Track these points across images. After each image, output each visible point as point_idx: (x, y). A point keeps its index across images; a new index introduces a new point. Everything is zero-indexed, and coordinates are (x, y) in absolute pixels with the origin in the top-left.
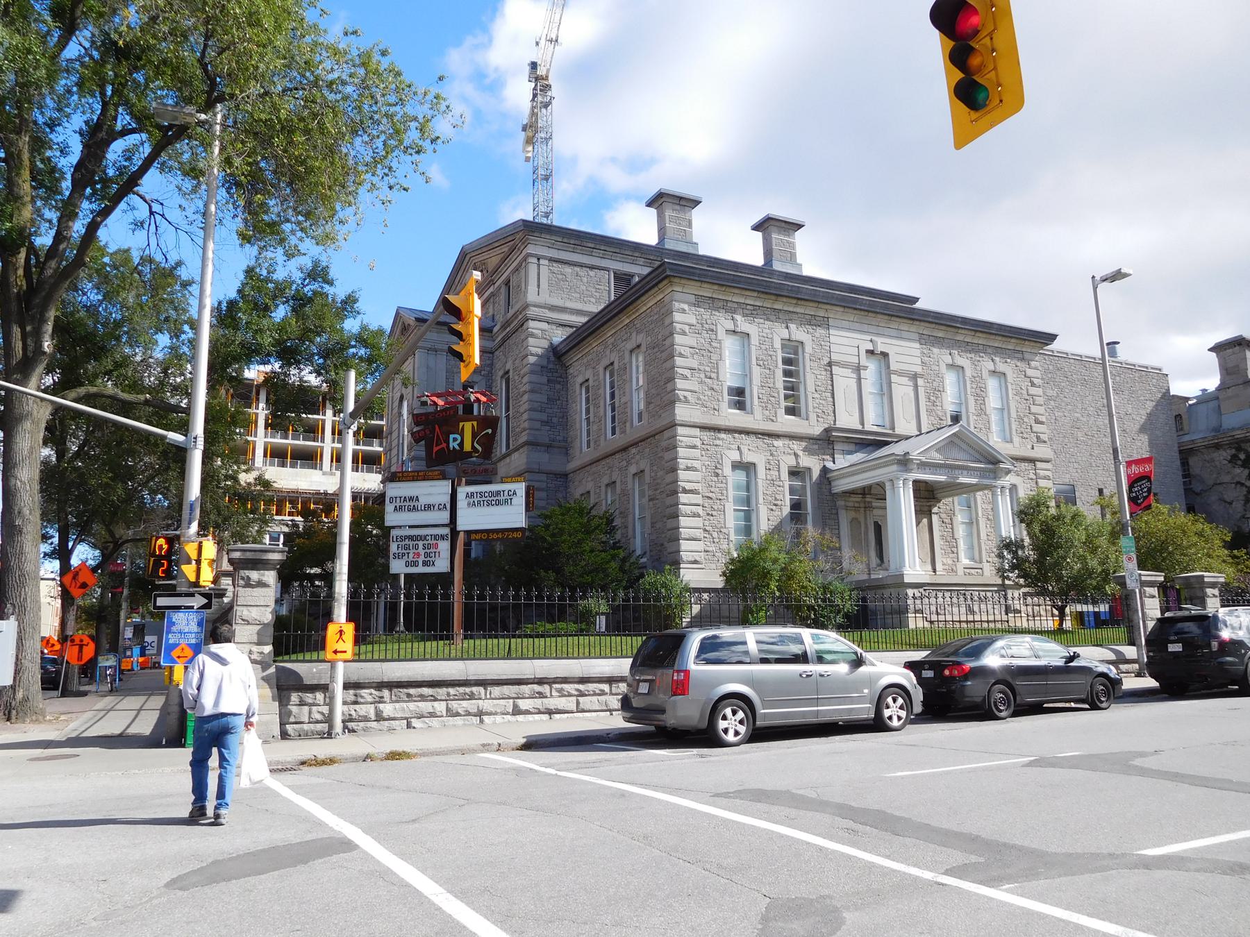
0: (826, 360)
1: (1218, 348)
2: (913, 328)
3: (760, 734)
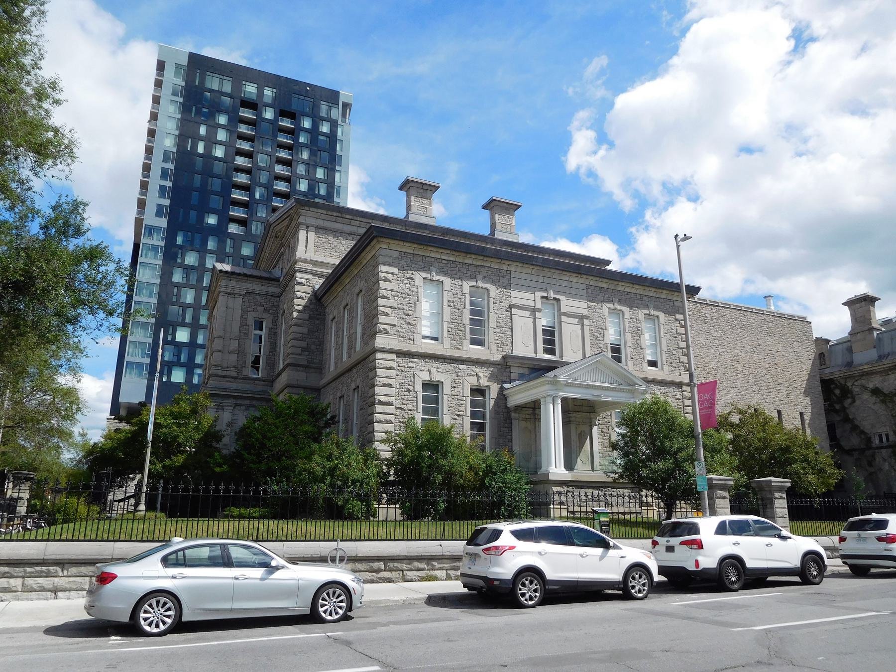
0: (507, 304)
1: (849, 303)
2: (582, 281)
3: (180, 627)
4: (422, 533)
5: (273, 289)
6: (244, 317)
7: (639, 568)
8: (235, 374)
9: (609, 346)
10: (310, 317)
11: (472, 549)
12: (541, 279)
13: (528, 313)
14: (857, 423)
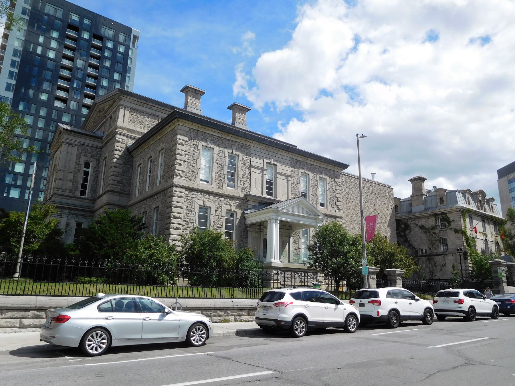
0: (248, 165)
2: (289, 155)
3: (111, 350)
4: (213, 294)
5: (97, 144)
6: (78, 158)
7: (352, 315)
8: (70, 194)
9: (301, 193)
10: (124, 163)
11: (264, 303)
12: (267, 152)
13: (259, 171)
14: (411, 243)
